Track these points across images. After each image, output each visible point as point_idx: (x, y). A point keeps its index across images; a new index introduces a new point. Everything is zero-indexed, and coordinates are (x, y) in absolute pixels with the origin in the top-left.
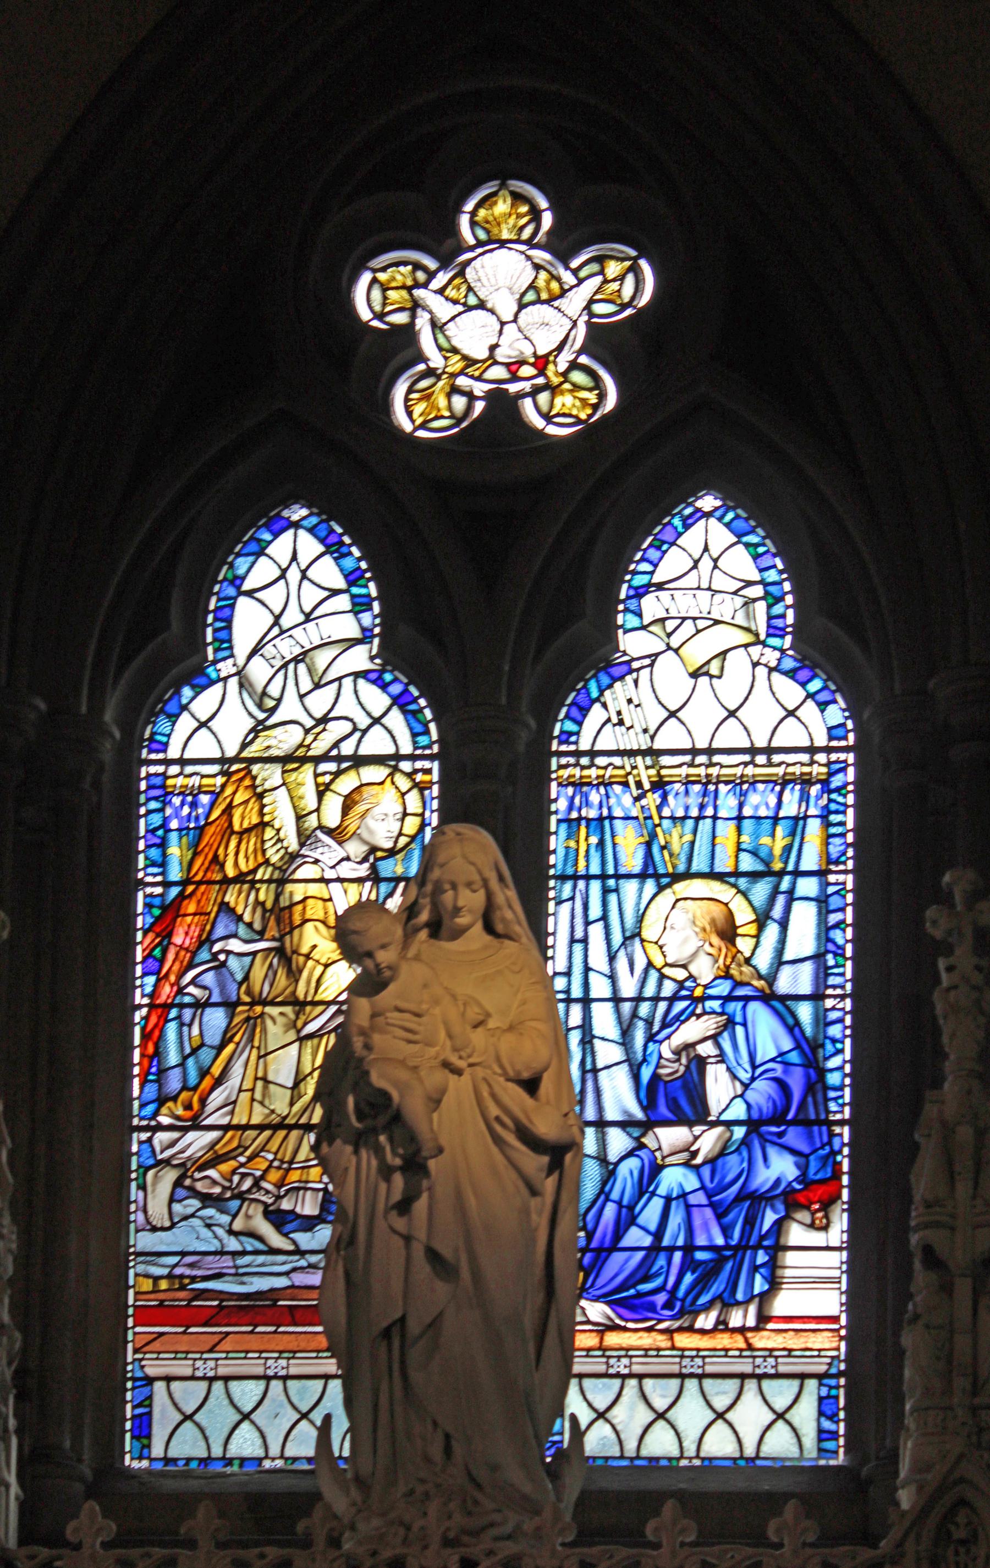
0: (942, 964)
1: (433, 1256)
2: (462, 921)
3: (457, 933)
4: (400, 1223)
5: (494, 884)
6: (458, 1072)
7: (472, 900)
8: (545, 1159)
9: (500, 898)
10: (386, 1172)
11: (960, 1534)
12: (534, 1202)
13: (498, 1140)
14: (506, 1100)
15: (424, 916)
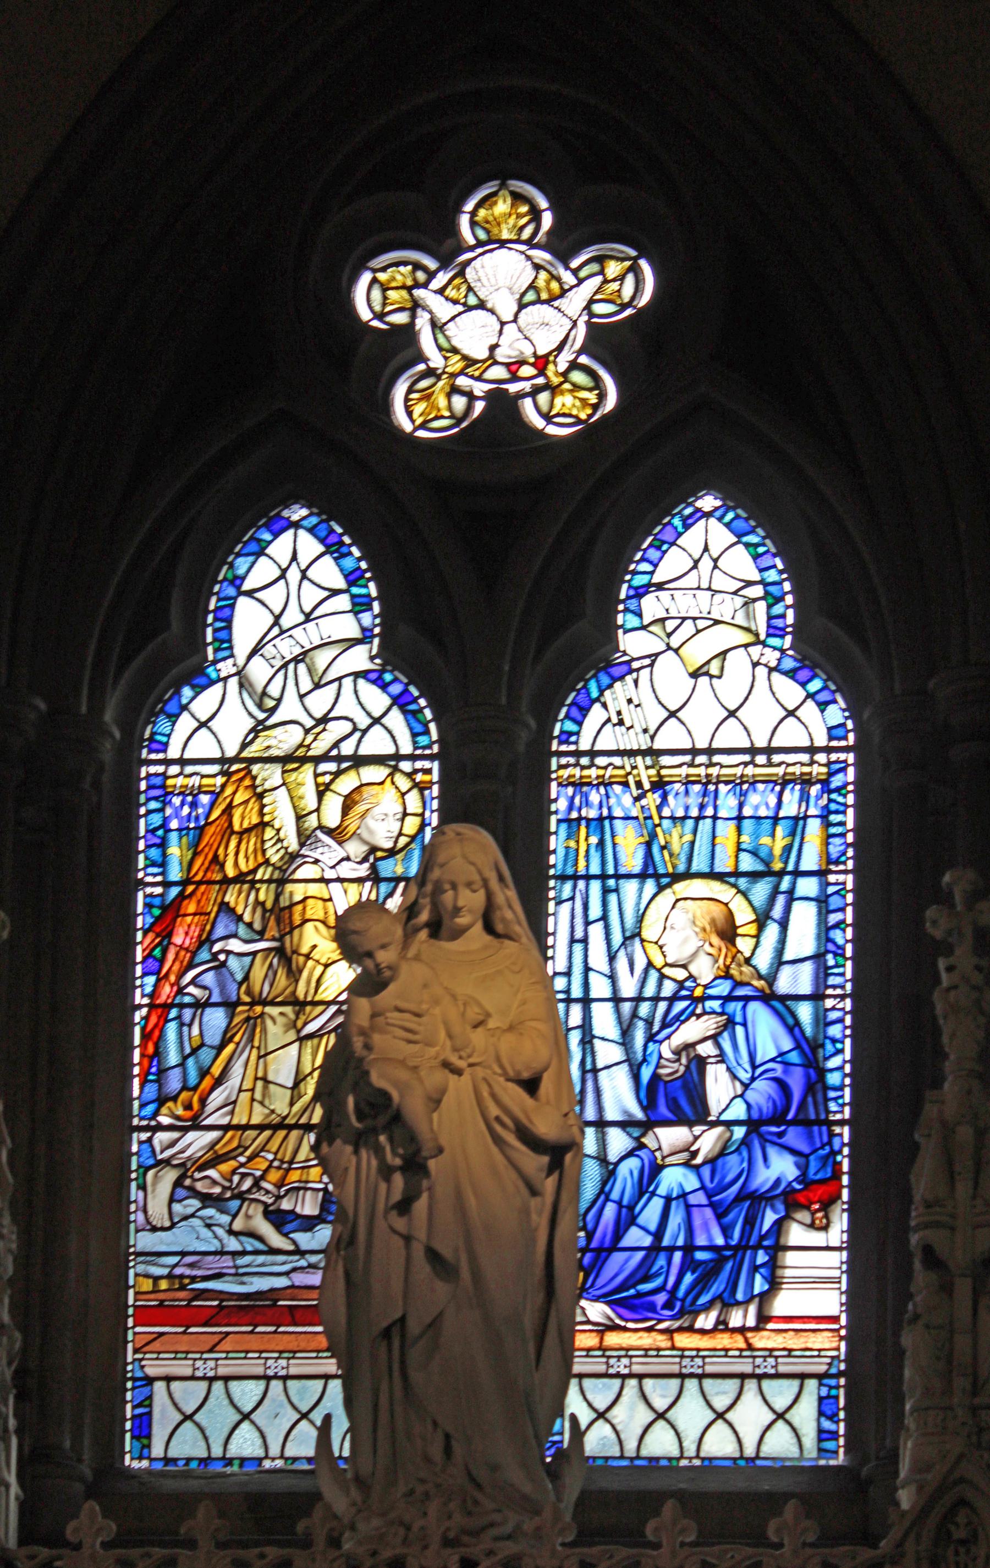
0: (942, 964)
1: (433, 1256)
2: (462, 921)
3: (457, 933)
4: (400, 1223)
5: (494, 884)
6: (458, 1072)
7: (472, 900)
8: (545, 1159)
9: (500, 898)
10: (386, 1172)
11: (960, 1534)
12: (534, 1202)
13: (498, 1140)
14: (506, 1100)
15: (424, 916)
